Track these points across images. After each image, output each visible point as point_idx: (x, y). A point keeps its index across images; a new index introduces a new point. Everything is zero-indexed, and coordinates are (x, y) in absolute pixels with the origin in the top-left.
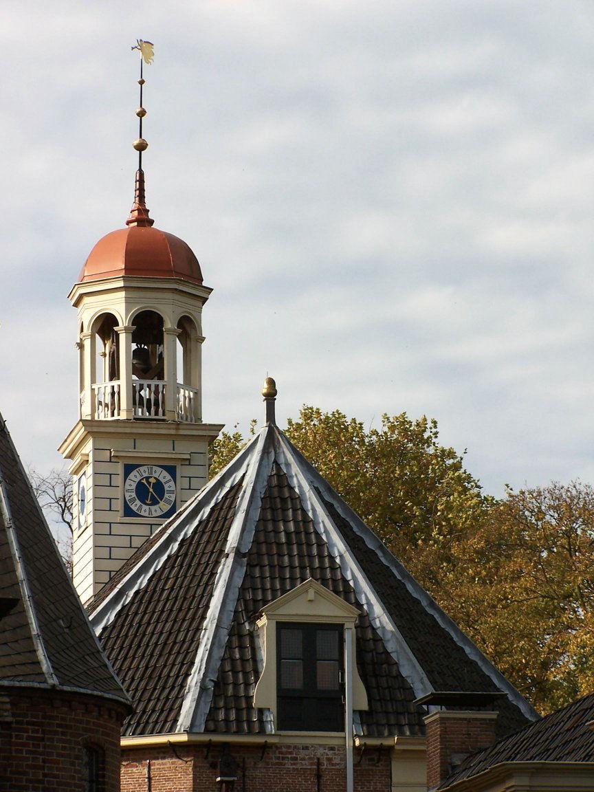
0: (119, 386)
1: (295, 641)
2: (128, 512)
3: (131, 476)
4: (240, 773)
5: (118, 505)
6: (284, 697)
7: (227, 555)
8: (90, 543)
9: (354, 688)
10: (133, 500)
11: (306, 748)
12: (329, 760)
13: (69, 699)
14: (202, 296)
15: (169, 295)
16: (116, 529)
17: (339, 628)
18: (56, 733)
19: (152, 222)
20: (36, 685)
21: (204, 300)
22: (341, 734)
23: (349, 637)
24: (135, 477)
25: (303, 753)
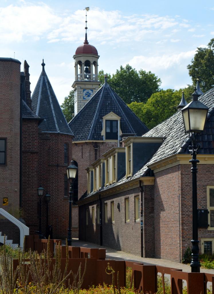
0: (91, 75)
1: (109, 123)
2: (84, 98)
3: (85, 92)
4: (98, 147)
5: (82, 97)
6: (107, 133)
7: (53, 110)
8: (77, 104)
9: (120, 131)
10: (85, 96)
11: (111, 143)
12: (115, 145)
13: (62, 135)
14: (98, 57)
15: (91, 57)
16: (82, 102)
17: (117, 121)
18: (59, 141)
19: (88, 43)
20: (56, 132)
21: (98, 58)
22: (117, 140)
23: (119, 122)
24: (85, 92)
25: (110, 144)
